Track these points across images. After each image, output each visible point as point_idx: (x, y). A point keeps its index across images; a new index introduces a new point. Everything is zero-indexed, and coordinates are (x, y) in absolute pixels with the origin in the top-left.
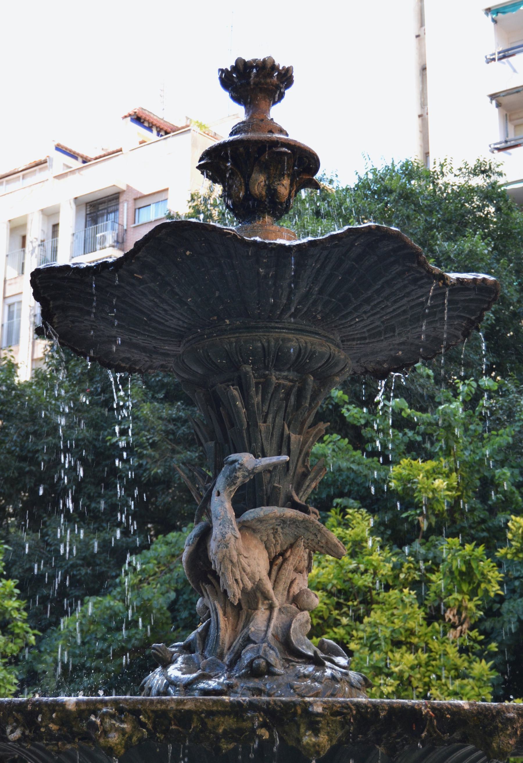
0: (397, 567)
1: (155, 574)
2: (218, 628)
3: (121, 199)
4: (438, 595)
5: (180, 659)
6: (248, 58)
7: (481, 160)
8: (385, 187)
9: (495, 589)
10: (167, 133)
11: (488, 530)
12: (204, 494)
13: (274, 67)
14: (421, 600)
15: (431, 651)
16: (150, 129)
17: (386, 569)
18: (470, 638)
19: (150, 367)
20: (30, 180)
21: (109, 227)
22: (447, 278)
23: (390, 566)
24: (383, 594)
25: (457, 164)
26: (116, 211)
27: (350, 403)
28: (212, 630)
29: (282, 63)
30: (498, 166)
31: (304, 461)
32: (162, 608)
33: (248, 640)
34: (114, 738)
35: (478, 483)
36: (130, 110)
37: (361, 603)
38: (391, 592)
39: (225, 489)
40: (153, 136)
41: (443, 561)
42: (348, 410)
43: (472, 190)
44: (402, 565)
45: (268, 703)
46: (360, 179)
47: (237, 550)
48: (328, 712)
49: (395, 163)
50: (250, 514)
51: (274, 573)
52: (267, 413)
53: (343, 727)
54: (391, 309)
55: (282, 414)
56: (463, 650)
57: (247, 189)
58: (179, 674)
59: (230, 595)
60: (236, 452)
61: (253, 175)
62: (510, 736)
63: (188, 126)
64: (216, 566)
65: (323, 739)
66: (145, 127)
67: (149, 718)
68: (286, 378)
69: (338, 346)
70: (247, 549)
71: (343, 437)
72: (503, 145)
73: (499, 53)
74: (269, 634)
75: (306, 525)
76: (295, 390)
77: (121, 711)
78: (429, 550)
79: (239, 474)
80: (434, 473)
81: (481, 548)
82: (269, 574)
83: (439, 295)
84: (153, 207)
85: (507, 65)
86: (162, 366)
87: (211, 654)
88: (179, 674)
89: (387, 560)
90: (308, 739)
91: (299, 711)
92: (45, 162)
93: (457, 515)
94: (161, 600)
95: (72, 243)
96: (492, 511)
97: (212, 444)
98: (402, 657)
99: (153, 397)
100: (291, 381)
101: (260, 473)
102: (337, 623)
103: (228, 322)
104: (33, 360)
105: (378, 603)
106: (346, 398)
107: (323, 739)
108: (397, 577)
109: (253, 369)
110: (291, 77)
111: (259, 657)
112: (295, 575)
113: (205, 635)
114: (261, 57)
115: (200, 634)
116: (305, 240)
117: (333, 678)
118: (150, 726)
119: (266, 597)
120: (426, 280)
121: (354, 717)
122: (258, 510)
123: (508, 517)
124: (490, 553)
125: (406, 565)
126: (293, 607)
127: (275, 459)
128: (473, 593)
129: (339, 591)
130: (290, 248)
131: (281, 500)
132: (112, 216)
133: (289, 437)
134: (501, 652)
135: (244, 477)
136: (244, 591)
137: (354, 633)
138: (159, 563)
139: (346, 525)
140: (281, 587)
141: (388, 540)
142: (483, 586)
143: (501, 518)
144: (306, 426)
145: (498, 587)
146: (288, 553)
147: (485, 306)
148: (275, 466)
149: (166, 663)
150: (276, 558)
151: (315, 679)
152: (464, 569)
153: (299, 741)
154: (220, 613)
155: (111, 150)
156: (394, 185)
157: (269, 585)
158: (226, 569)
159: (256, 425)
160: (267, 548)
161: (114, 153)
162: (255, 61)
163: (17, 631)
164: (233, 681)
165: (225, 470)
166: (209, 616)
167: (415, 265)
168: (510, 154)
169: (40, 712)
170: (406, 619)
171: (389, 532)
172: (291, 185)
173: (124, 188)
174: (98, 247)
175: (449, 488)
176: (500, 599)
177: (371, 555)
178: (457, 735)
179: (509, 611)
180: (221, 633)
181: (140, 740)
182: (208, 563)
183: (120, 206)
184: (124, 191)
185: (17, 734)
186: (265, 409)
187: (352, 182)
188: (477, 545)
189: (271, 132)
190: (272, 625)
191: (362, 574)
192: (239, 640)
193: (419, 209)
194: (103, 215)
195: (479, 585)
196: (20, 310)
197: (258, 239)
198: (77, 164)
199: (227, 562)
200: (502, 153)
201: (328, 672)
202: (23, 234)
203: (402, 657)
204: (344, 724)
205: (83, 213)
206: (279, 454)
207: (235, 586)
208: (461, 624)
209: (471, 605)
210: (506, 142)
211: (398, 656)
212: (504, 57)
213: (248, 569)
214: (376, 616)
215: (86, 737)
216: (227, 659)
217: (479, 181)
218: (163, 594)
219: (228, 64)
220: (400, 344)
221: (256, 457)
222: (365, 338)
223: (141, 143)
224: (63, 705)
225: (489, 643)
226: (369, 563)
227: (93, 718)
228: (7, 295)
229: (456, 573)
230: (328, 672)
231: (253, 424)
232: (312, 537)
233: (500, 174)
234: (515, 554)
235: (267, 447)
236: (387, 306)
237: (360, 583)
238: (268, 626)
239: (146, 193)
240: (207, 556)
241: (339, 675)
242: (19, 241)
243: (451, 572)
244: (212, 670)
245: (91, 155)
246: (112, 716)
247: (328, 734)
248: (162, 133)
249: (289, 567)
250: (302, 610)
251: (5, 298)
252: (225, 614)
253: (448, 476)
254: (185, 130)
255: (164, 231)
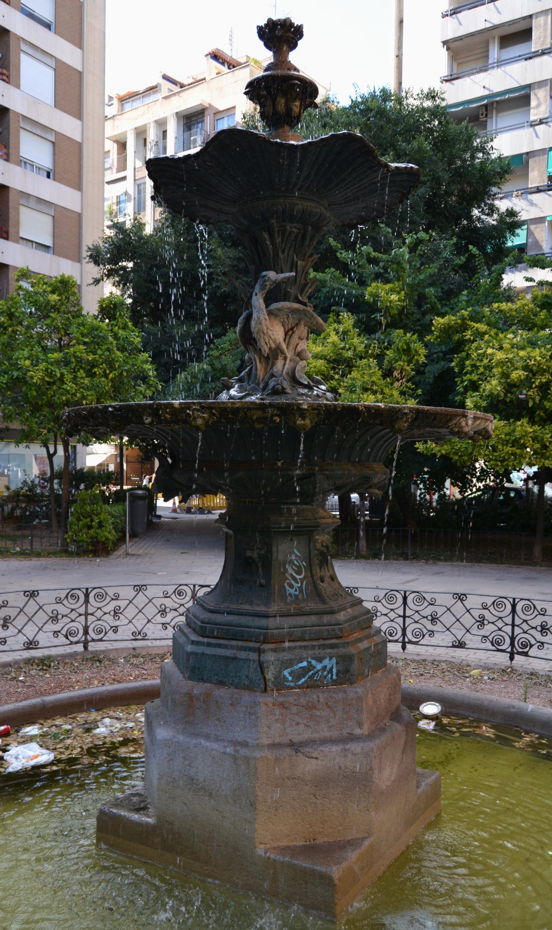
0: (367, 347)
1: (229, 350)
2: (256, 369)
3: (206, 113)
4: (390, 362)
5: (236, 386)
6: (274, 18)
7: (432, 89)
8: (368, 107)
9: (422, 359)
10: (234, 67)
11: (421, 325)
12: (248, 295)
13: (291, 25)
14: (380, 365)
15: (384, 394)
16: (223, 64)
17: (361, 348)
18: (406, 386)
19: (219, 221)
20: (148, 100)
21: (199, 132)
22: (390, 166)
23: (363, 346)
24: (359, 362)
25: (416, 91)
26: (203, 121)
27: (342, 249)
28: (253, 371)
29: (297, 22)
30: (442, 94)
31: (305, 277)
32: (233, 370)
33: (272, 376)
34: (199, 422)
35: (416, 297)
36: (209, 50)
37: (346, 367)
38: (363, 360)
39: (260, 292)
40: (225, 69)
41: (394, 343)
42: (341, 253)
43: (424, 110)
44: (370, 345)
45: (279, 404)
46: (352, 101)
47: (266, 326)
48: (310, 408)
49: (376, 90)
50: (274, 306)
51: (287, 340)
52: (285, 248)
53: (318, 417)
54: (357, 186)
55: (293, 248)
56: (402, 393)
57: (274, 108)
58: (236, 393)
59: (263, 351)
60: (266, 270)
61: (278, 99)
62: (405, 422)
63: (247, 62)
64: (255, 335)
65: (308, 422)
66: (220, 63)
67: (217, 411)
68: (295, 227)
69: (326, 208)
70: (272, 326)
71: (337, 270)
72: (449, 78)
73: (451, 10)
74: (284, 373)
75: (305, 313)
76: (301, 234)
77: (203, 407)
78: (386, 336)
79: (268, 283)
80: (392, 290)
81: (416, 336)
82: (285, 340)
83: (384, 178)
84: (226, 119)
85: (456, 20)
86: (226, 220)
87: (253, 383)
88: (236, 393)
89: (362, 342)
90: (300, 422)
91: (295, 408)
92: (156, 87)
93: (403, 317)
94: (232, 365)
95: (175, 144)
96: (424, 314)
97: (253, 266)
98: (368, 397)
99: (225, 245)
100: (298, 229)
101: (279, 283)
102: (332, 378)
103: (262, 193)
104: (154, 221)
105: (356, 367)
106: (339, 246)
107: (308, 422)
108: (367, 352)
109: (276, 222)
110: (302, 32)
111: (278, 384)
112: (300, 341)
113: (249, 373)
114: (282, 17)
115: (247, 372)
116: (306, 142)
117: (318, 395)
118: (218, 416)
119: (283, 353)
120: (377, 168)
121: (324, 411)
122: (278, 304)
123: (432, 318)
124: (421, 338)
125: (373, 345)
126: (298, 358)
127: (287, 275)
128: (410, 362)
129: (334, 360)
130: (297, 146)
131: (292, 297)
132: (200, 125)
133: (297, 262)
134: (423, 394)
135: (271, 285)
136: (270, 349)
137: (342, 383)
138: (231, 344)
139: (339, 322)
140: (291, 347)
141: (363, 331)
142: (416, 357)
143: (428, 317)
144: (307, 256)
145: (424, 358)
146: (295, 329)
147: (412, 184)
148: (289, 278)
149: (229, 388)
150: (288, 331)
151: (308, 396)
152: (405, 347)
153: (295, 423)
154: (258, 361)
155: (199, 78)
156: (374, 105)
157: (284, 346)
158: (260, 336)
159: (278, 255)
160: (283, 326)
161: (200, 81)
162: (279, 20)
163: (151, 382)
164: (264, 396)
165: (260, 281)
166: (252, 363)
167: (371, 158)
168: (453, 84)
169: (161, 408)
170: (371, 376)
171: (363, 327)
172: (301, 105)
173: (207, 105)
174: (192, 146)
175: (399, 300)
176: (425, 365)
177: (353, 339)
178: (377, 421)
179: (429, 372)
180: (258, 372)
181: (213, 423)
182: (251, 333)
183: (205, 118)
184: (207, 108)
185: (149, 420)
186: (283, 246)
187: (347, 103)
188: (413, 334)
189: (289, 69)
190: (286, 368)
191: (347, 350)
192: (268, 375)
193: (389, 121)
194: (194, 125)
195: (413, 357)
196: (145, 188)
197: (278, 140)
198: (177, 89)
199: (261, 333)
200: (448, 83)
201: (315, 392)
202: (144, 137)
203: (368, 397)
204: (318, 415)
205: (182, 123)
206: (291, 272)
207: (265, 346)
208: (402, 379)
209: (408, 368)
210: (451, 75)
211: (365, 396)
212: (454, 13)
213: (273, 337)
214: (354, 374)
215: (185, 422)
216: (261, 386)
217: (428, 104)
218: (233, 362)
219: (263, 22)
220: (363, 208)
221: (277, 273)
222: (342, 204)
223: (217, 74)
224: (172, 404)
225: (417, 389)
226: (352, 344)
227: (188, 411)
228: (137, 178)
229: (401, 350)
230: (315, 392)
231: (276, 255)
232: (308, 320)
233: (443, 99)
234: (435, 339)
235: (284, 268)
236: (354, 184)
237: (346, 355)
238: (283, 368)
239: (221, 109)
240: (250, 330)
241: (321, 394)
242: (142, 142)
243: (398, 349)
244: (253, 391)
245: (186, 82)
246: (198, 410)
247: (310, 419)
248: (231, 67)
249: (296, 336)
250: (302, 360)
251: (135, 180)
252: (260, 362)
253: (399, 293)
254: (246, 65)
255: (223, 135)
